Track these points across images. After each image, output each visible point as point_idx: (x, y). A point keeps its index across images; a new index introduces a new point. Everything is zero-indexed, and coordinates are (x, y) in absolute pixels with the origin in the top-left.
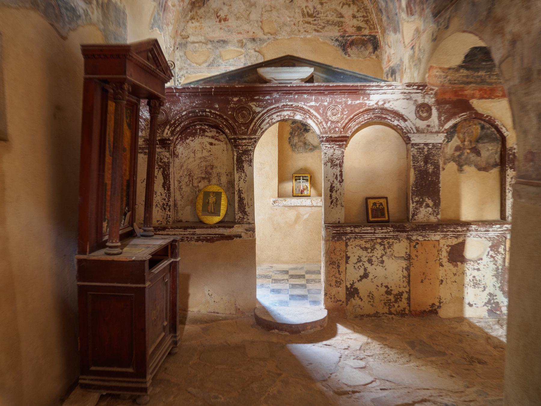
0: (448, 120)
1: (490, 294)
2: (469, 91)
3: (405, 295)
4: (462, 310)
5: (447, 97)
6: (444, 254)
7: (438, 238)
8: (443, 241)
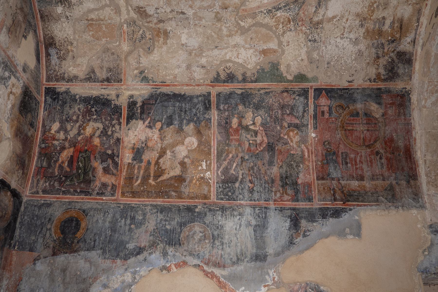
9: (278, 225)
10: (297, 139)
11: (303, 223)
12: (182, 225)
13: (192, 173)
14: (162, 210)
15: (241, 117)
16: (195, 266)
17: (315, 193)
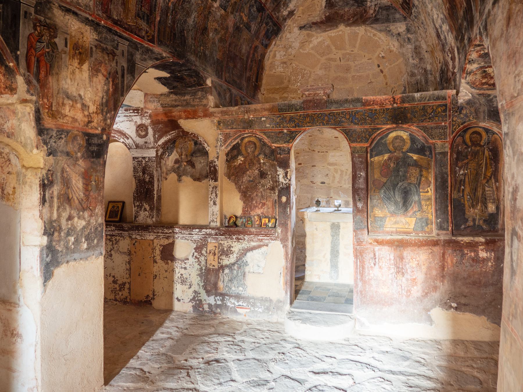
0: (160, 137)
1: (195, 292)
2: (176, 112)
3: (127, 286)
4: (171, 304)
6: (158, 252)
7: (152, 238)
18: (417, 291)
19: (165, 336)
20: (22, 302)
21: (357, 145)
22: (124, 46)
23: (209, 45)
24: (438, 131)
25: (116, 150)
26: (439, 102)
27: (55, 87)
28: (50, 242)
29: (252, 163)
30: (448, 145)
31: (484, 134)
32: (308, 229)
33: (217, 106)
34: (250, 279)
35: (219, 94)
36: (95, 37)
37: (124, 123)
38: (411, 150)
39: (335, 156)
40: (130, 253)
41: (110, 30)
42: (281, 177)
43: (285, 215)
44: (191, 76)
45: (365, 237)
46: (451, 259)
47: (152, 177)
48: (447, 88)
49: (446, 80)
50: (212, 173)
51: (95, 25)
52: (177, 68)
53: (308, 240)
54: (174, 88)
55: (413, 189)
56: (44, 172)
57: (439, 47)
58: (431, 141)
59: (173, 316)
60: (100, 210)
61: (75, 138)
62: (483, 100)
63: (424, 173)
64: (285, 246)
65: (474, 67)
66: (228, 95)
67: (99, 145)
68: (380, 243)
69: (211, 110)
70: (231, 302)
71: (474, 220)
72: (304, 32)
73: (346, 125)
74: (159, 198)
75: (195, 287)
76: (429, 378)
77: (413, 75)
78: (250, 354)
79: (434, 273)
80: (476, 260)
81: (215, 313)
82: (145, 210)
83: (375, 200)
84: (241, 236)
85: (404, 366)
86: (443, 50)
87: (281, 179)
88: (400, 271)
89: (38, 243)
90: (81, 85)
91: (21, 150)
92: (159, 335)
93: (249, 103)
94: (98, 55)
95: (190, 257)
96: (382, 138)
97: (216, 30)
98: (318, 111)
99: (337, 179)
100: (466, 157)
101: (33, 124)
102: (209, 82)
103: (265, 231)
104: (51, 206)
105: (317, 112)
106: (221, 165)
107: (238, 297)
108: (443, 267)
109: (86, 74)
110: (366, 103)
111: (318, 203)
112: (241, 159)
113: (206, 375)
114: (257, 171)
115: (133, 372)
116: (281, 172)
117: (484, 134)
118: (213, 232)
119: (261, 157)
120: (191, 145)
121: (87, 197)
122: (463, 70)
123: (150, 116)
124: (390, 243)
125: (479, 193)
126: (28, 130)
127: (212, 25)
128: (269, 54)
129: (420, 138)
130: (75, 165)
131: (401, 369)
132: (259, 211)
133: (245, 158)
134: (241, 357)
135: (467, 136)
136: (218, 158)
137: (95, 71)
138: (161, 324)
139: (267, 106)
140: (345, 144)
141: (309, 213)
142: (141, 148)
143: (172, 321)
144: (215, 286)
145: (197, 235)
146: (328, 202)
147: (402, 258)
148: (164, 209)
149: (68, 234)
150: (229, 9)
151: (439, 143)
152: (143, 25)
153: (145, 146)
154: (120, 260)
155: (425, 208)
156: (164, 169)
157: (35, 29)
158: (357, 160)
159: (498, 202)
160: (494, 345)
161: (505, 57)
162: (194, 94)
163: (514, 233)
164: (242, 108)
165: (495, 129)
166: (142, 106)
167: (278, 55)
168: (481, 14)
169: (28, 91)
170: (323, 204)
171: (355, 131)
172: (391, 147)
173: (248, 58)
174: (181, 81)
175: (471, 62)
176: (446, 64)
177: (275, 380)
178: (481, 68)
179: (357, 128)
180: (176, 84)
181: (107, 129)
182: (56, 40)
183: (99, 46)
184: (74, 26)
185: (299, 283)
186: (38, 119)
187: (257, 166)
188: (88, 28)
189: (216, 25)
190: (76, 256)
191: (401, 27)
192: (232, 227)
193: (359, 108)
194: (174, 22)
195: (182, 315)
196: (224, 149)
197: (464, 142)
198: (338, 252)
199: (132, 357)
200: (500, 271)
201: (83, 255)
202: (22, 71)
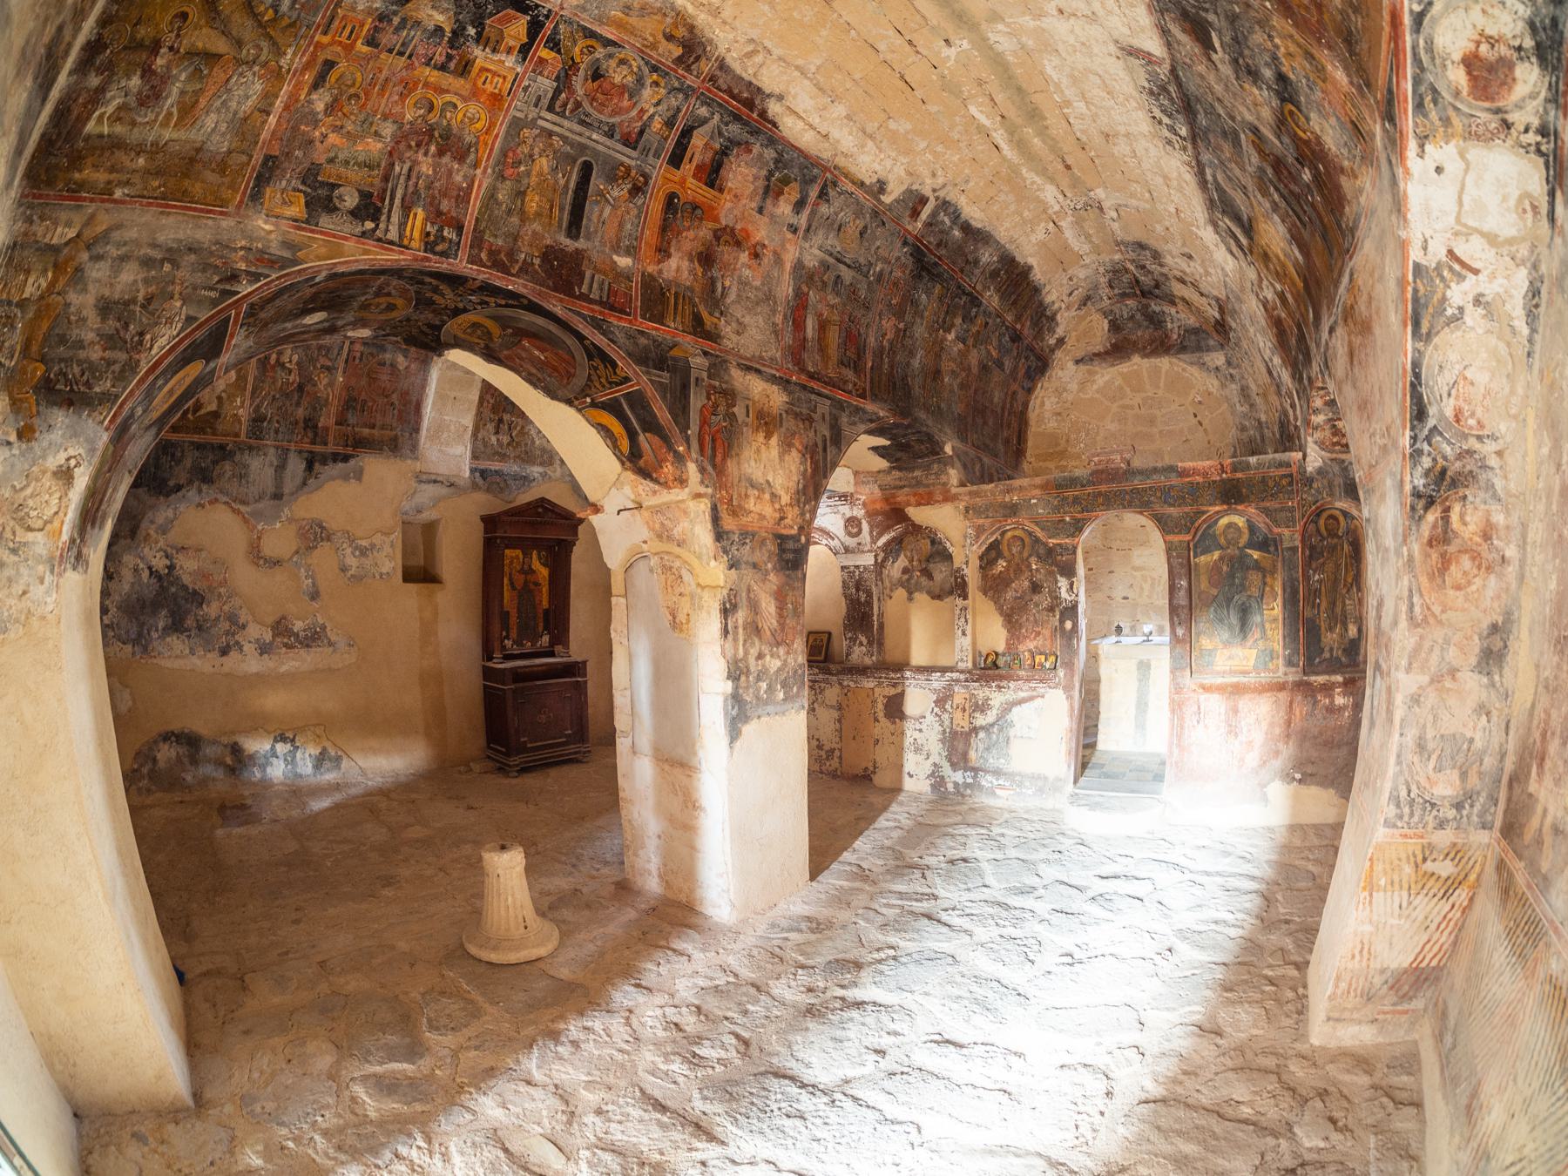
0: (880, 535)
1: (935, 765)
2: (901, 497)
3: (837, 753)
4: (900, 780)
5: (878, 506)
6: (880, 706)
7: (871, 685)
8: (875, 688)
9: (296, 466)
10: (325, 382)
11: (317, 465)
12: (215, 463)
13: (228, 411)
14: (199, 447)
15: (280, 353)
16: (226, 503)
17: (331, 438)
18: (1253, 759)
19: (891, 824)
20: (704, 767)
21: (1176, 539)
22: (824, 407)
23: (945, 395)
24: (1283, 514)
25: (818, 556)
26: (1283, 471)
27: (736, 473)
28: (736, 688)
29: (1019, 571)
30: (1297, 536)
31: (1341, 519)
32: (1105, 671)
33: (962, 485)
34: (1016, 747)
35: (965, 466)
36: (785, 399)
37: (829, 517)
38: (1251, 545)
39: (1140, 556)
40: (840, 708)
41: (804, 387)
42: (1063, 590)
43: (1073, 652)
44: (922, 442)
45: (1187, 681)
46: (1301, 708)
47: (869, 594)
48: (1291, 450)
49: (1288, 438)
50: (959, 588)
51: (784, 383)
52: (901, 431)
53: (1104, 688)
54: (897, 460)
55: (1254, 605)
56: (725, 592)
57: (1273, 388)
58: (1276, 530)
59: (901, 797)
60: (799, 645)
61: (763, 542)
62: (1336, 469)
63: (1268, 580)
64: (1070, 697)
65: (1319, 419)
66: (978, 467)
67: (796, 551)
68: (1207, 689)
69: (954, 490)
70: (986, 781)
71: (1331, 649)
72: (1083, 367)
73: (1157, 507)
74: (881, 626)
75: (935, 758)
76: (1253, 878)
77: (1243, 429)
78: (1013, 853)
79: (1277, 731)
80: (1332, 710)
81: (963, 796)
82: (861, 644)
83: (1202, 624)
84: (1004, 683)
85: (1225, 865)
86: (1279, 393)
87: (1064, 594)
88: (1232, 731)
89: (720, 690)
90: (769, 466)
91: (695, 562)
92: (882, 822)
93: (1010, 478)
94: (790, 423)
95: (928, 714)
96: (1209, 527)
97: (953, 372)
98: (1114, 487)
99: (1146, 593)
100: (1322, 553)
101: (709, 526)
102: (948, 449)
103: (1039, 674)
104: (735, 640)
105: (1113, 488)
106: (972, 574)
107: (997, 773)
108: (1288, 723)
109: (774, 452)
110: (1183, 473)
111: (1119, 630)
112: (1002, 564)
113: (948, 877)
114: (1027, 583)
115: (848, 868)
116: (1063, 583)
117: (1341, 519)
118: (962, 677)
119: (1033, 560)
120: (926, 545)
121: (782, 625)
122: (1308, 423)
123: (864, 504)
124: (1221, 689)
125: (1338, 610)
126: (703, 535)
127: (947, 366)
128: (1034, 403)
129: (1262, 525)
130: (764, 581)
131: (1220, 868)
132: (1031, 645)
133: (1009, 562)
134: (999, 857)
135: (1322, 522)
136: (967, 563)
137: (787, 445)
138: (885, 808)
139: (1038, 480)
140: (1156, 536)
141: (1106, 646)
142: (853, 552)
143: (901, 804)
144: (965, 756)
145: (938, 682)
146: (1133, 628)
147: (1236, 711)
148: (889, 642)
149: (758, 679)
150: (970, 342)
151: (1286, 532)
152: (849, 374)
153: (858, 550)
154: (827, 717)
155: (1269, 633)
156: (887, 583)
157: (709, 398)
158: (1175, 562)
159: (1360, 622)
160: (1338, 827)
161: (1355, 408)
162: (928, 468)
163: (1377, 667)
164: (1002, 485)
165: (1355, 512)
166: (851, 489)
167: (1047, 403)
168: (1318, 345)
169: (702, 482)
170: (1126, 631)
171: (1170, 516)
172: (1222, 541)
173: (1003, 409)
174: (908, 450)
175: (1316, 411)
176: (1285, 413)
177: (1045, 887)
178: (1330, 420)
179: (1173, 511)
180: (899, 455)
181: (806, 527)
182: (735, 410)
183: (791, 411)
184: (756, 387)
185: (1087, 752)
186: (716, 519)
187: (1027, 574)
188: (775, 387)
189: (953, 365)
190: (770, 709)
191: (1218, 358)
192: (990, 669)
193: (1175, 481)
194: (892, 367)
195: (916, 798)
196: (977, 550)
197: (1318, 531)
198: (1146, 704)
199: (846, 849)
200: (1356, 723)
201: (779, 708)
202: (694, 455)
